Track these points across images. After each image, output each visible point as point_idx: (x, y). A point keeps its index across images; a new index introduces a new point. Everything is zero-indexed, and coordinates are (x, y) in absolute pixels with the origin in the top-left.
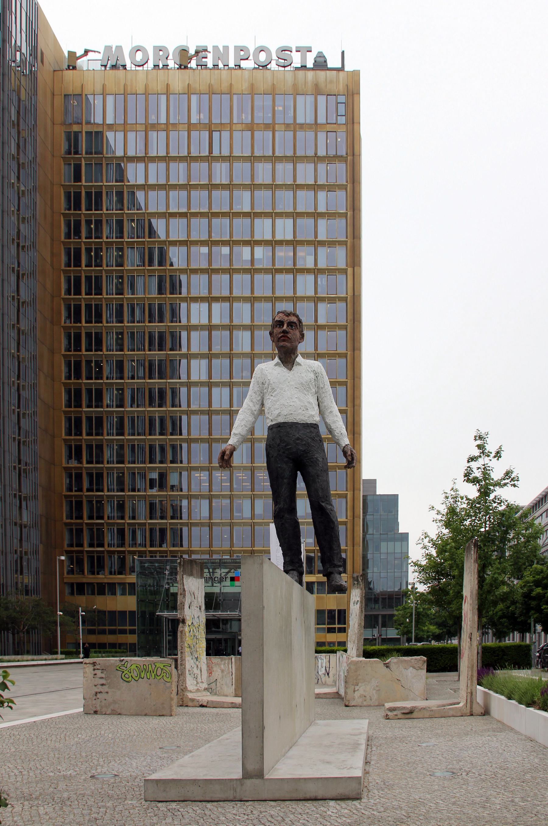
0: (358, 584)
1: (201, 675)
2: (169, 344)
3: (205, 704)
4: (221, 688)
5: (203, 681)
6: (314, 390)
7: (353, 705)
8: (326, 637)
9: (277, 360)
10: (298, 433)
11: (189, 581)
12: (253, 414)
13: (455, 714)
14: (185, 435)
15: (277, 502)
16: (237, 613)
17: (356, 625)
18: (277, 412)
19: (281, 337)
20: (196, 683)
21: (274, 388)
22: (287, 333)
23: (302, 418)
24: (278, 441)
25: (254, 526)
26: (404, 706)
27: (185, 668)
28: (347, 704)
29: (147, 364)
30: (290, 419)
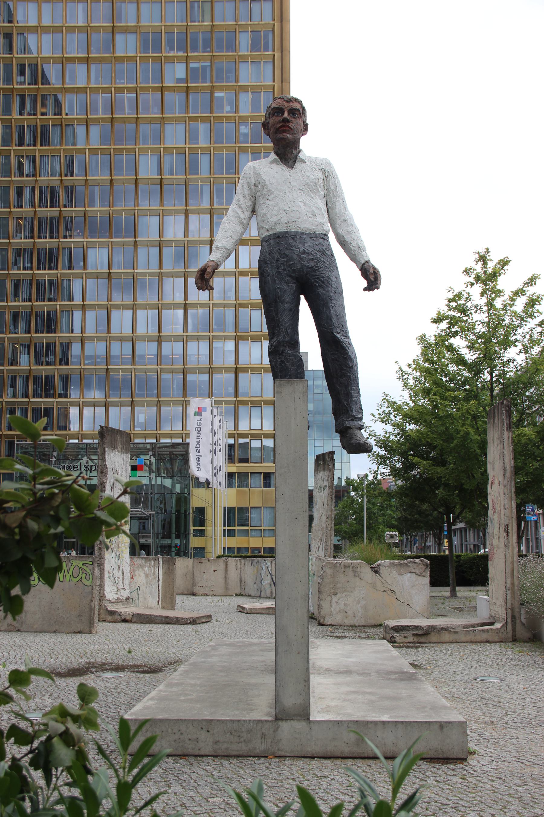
0: (324, 464)
1: (123, 579)
2: (63, 201)
3: (128, 618)
4: (145, 599)
5: (125, 587)
6: (323, 193)
7: (329, 623)
8: (248, 542)
9: (273, 156)
10: (304, 245)
11: (112, 455)
12: (242, 223)
13: (490, 639)
14: (78, 300)
15: (274, 334)
16: (140, 510)
17: (324, 517)
18: (275, 219)
19: (280, 127)
20: (116, 590)
21: (270, 190)
22: (288, 121)
23: (309, 226)
24: (276, 256)
25: (160, 405)
26: (416, 624)
27: (103, 570)
28: (321, 622)
29: (36, 222)
30: (292, 228)
